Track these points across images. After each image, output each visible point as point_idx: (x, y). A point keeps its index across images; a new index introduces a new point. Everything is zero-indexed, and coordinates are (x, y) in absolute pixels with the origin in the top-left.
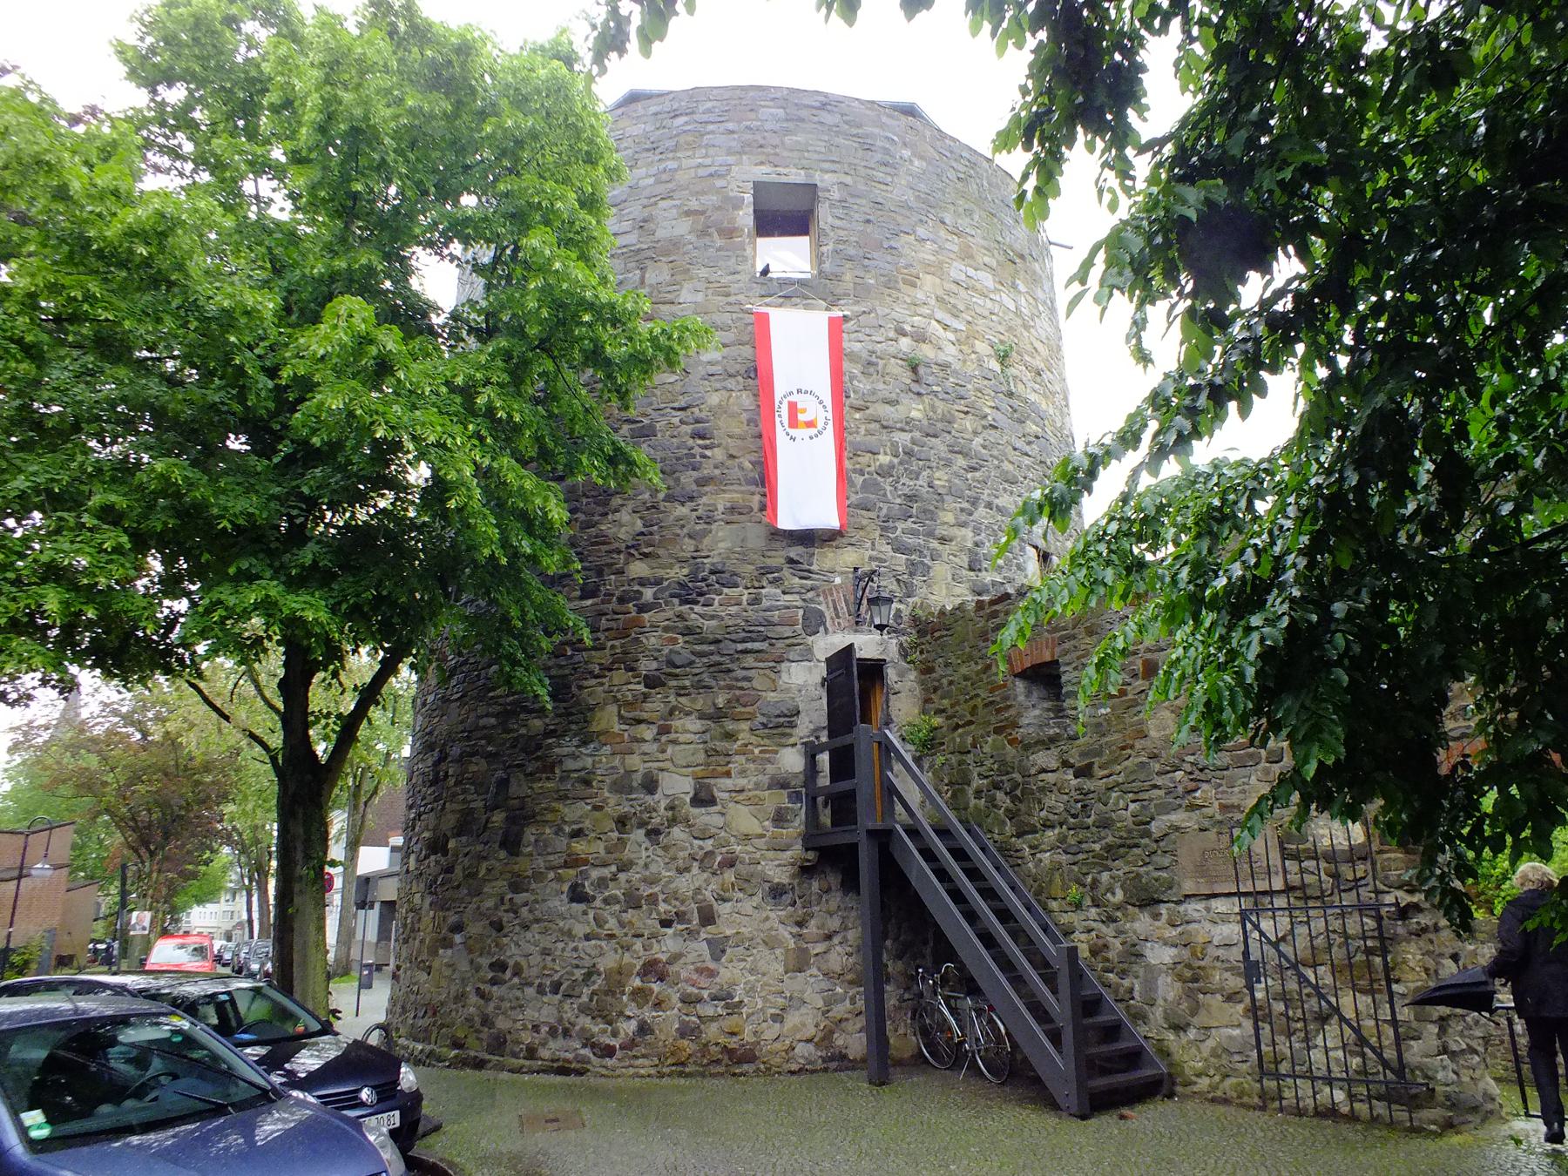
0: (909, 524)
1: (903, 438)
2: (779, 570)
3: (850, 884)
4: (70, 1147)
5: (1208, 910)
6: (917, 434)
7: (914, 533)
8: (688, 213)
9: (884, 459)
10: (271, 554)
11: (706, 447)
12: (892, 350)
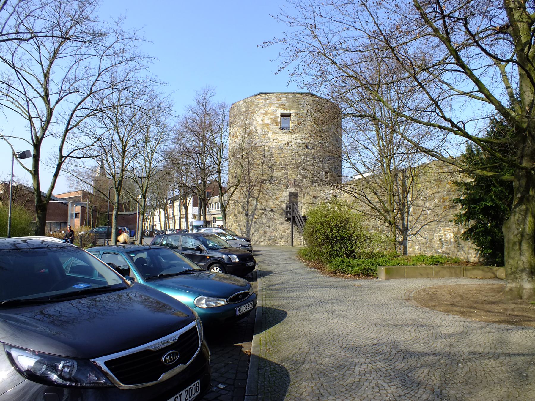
0: (303, 171)
9: (300, 161)
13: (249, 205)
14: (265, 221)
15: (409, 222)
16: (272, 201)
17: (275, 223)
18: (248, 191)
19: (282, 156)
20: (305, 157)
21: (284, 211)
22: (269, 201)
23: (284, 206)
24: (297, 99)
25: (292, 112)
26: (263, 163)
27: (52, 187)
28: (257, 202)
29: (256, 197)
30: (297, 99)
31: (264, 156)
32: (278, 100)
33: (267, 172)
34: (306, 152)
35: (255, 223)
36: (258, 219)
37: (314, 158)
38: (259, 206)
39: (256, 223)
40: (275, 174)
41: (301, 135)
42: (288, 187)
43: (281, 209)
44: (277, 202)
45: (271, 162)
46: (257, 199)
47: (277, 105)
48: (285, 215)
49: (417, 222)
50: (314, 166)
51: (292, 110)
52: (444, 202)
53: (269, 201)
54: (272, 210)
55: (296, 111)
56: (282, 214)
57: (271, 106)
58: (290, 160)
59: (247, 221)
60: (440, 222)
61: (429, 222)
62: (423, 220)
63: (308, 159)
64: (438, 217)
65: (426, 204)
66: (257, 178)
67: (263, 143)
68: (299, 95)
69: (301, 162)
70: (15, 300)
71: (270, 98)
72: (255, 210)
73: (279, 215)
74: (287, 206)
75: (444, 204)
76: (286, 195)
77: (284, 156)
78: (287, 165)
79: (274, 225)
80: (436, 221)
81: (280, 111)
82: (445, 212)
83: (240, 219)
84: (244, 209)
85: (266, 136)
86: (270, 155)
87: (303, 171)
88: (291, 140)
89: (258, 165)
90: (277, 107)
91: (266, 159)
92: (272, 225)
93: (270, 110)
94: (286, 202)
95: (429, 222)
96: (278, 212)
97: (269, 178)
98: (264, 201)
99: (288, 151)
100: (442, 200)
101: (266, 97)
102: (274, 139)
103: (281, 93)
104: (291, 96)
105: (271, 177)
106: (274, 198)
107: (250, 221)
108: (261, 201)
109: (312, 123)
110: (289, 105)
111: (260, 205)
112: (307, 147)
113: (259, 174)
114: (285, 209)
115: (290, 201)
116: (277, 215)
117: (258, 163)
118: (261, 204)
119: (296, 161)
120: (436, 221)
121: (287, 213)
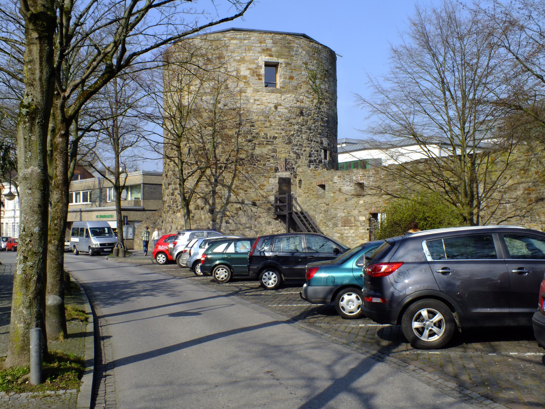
0: (297, 148)
1: (296, 127)
2: (269, 158)
3: (285, 222)
4: (113, 282)
5: (20, 27)
6: (300, 126)
7: (298, 149)
8: (249, 69)
9: (292, 133)
10: (32, 113)
11: (254, 129)
12: (295, 106)
13: (216, 196)
14: (244, 220)
15: (480, 218)
16: (254, 190)
17: (259, 223)
18: (214, 176)
19: (268, 124)
20: (299, 128)
21: (272, 205)
22: (248, 190)
23: (272, 199)
24: (288, 43)
25: (280, 61)
26: (238, 134)
27: (125, 183)
28: (229, 192)
29: (227, 184)
30: (288, 43)
31: (240, 124)
32: (261, 43)
33: (246, 148)
34: (300, 119)
35: (227, 222)
36: (233, 217)
37: (310, 129)
38: (233, 198)
39: (229, 223)
40: (258, 151)
41: (293, 96)
42: (276, 170)
43: (269, 202)
44: (261, 191)
45: (252, 134)
46: (230, 188)
47: (259, 49)
48: (273, 210)
49: (492, 218)
50: (311, 141)
51: (282, 58)
52: (530, 194)
53: (248, 190)
54: (254, 204)
55: (287, 60)
56: (269, 209)
57: (249, 50)
58: (279, 132)
59: (214, 220)
60: (524, 217)
61: (509, 218)
62: (501, 215)
63: (303, 131)
64: (521, 211)
65: (504, 196)
66: (230, 156)
67: (238, 105)
68: (290, 38)
69: (294, 134)
70: (493, 313)
71: (249, 38)
72: (227, 203)
73: (264, 211)
74: (276, 199)
75: (530, 196)
76: (273, 182)
77: (271, 125)
78: (275, 138)
79: (258, 226)
80: (518, 216)
81: (263, 59)
82: (531, 206)
83: (201, 218)
84: (206, 201)
85: (243, 94)
86: (249, 123)
87: (297, 148)
88: (280, 102)
89: (231, 137)
90: (259, 52)
91: (244, 129)
92: (255, 226)
93: (249, 55)
94: (274, 192)
95: (509, 218)
96: (263, 207)
97: (248, 156)
98: (241, 191)
99: (275, 119)
100: (526, 192)
101: (242, 36)
102: (255, 100)
103: (266, 32)
104: (278, 37)
105: (252, 155)
106: (257, 186)
107: (218, 221)
108: (236, 190)
109: (308, 79)
110: (277, 51)
111: (235, 197)
112: (302, 113)
113: (233, 151)
114: (273, 203)
115: (281, 191)
116: (262, 210)
117: (230, 133)
118: (237, 195)
119: (288, 133)
120: (518, 216)
121: (276, 207)
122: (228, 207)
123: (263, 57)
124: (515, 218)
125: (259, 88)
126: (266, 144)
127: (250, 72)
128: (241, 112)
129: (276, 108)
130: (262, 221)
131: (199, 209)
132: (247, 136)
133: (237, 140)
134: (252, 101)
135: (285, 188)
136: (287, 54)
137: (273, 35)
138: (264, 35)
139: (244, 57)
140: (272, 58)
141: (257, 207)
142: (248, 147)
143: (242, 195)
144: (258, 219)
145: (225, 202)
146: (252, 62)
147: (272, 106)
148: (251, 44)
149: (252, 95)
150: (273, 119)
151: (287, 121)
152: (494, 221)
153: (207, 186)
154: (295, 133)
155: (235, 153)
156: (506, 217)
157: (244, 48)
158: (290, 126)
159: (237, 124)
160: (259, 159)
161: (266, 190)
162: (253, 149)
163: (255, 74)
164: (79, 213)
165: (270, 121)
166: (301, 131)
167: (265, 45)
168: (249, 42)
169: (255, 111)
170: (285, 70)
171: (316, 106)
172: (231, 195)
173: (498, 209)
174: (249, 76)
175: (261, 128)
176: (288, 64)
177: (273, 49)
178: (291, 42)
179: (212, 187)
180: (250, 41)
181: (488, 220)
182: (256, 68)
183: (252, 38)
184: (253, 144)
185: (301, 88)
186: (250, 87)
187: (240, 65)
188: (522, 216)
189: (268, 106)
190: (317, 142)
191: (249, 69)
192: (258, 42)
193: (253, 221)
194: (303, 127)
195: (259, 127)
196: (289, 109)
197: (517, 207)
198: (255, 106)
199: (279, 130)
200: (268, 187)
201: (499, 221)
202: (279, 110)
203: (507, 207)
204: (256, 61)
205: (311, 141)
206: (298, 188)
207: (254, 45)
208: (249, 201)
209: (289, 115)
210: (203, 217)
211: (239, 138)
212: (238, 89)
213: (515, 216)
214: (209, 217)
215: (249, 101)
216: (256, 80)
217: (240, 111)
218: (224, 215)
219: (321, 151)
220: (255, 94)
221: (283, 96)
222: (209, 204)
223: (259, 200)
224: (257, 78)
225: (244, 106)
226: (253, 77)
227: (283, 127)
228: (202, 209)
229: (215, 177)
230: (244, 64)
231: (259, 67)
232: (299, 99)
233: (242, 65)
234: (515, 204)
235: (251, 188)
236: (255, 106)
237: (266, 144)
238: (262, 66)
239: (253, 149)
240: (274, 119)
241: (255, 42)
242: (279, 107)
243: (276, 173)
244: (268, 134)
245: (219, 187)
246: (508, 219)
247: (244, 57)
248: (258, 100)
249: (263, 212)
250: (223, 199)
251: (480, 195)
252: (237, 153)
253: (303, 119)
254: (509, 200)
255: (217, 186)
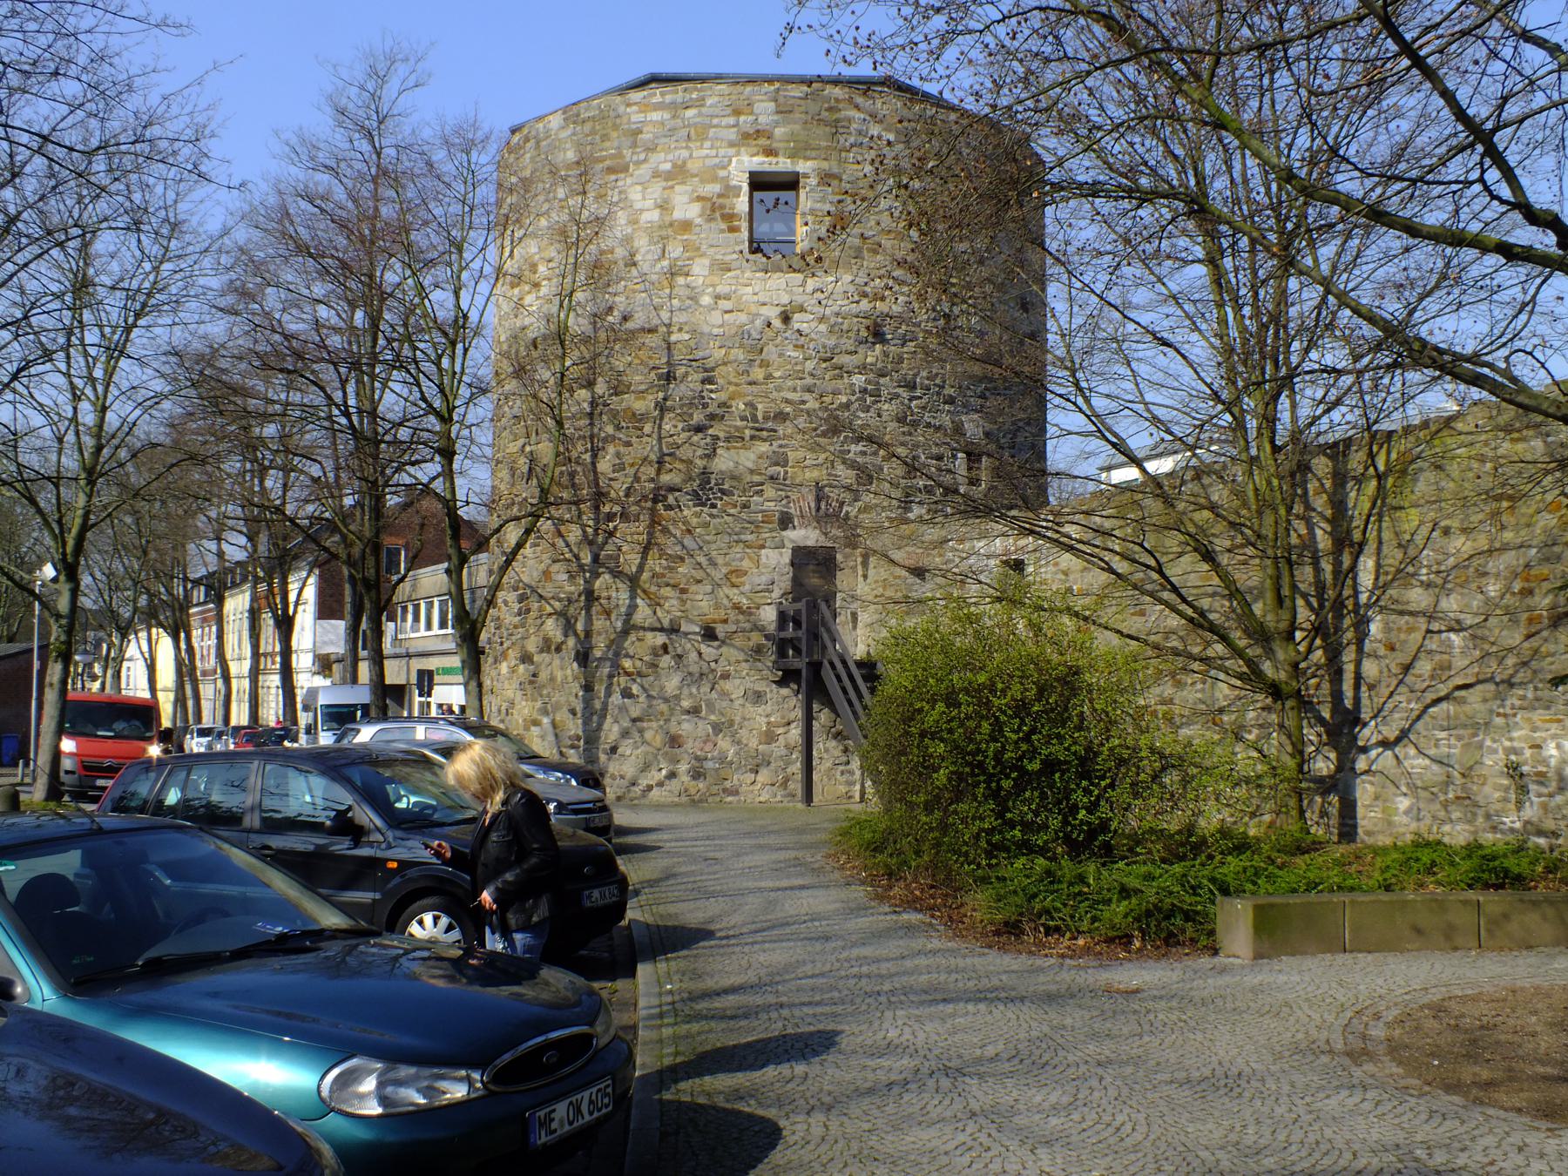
0: (860, 448)
2: (762, 484)
7: (864, 453)
8: (699, 199)
13: (596, 609)
15: (1364, 688)
17: (724, 694)
19: (758, 373)
20: (868, 382)
21: (767, 637)
23: (769, 615)
24: (830, 109)
25: (802, 166)
26: (662, 408)
28: (633, 597)
29: (627, 570)
30: (830, 109)
32: (737, 113)
34: (873, 355)
35: (627, 694)
38: (643, 613)
40: (724, 461)
41: (848, 278)
42: (785, 522)
43: (757, 628)
45: (705, 406)
46: (634, 581)
47: (732, 134)
48: (770, 658)
49: (1402, 689)
51: (807, 158)
52: (1531, 592)
54: (709, 634)
55: (825, 165)
56: (758, 650)
57: (702, 138)
59: (588, 688)
60: (1512, 685)
62: (1432, 677)
67: (665, 315)
68: (837, 91)
72: (625, 632)
75: (1530, 601)
76: (774, 562)
77: (769, 377)
80: (1491, 679)
81: (749, 161)
82: (1535, 642)
84: (569, 627)
85: (681, 280)
88: (799, 299)
90: (732, 144)
91: (679, 391)
92: (710, 705)
93: (701, 155)
94: (776, 594)
98: (666, 591)
99: (784, 355)
100: (1517, 587)
102: (718, 297)
103: (752, 80)
105: (705, 474)
107: (600, 689)
108: (653, 589)
110: (792, 137)
111: (648, 611)
112: (877, 335)
114: (772, 628)
115: (798, 588)
117: (640, 406)
119: (828, 399)
120: (1491, 679)
121: (782, 646)
122: (630, 644)
123: (746, 158)
124: (1479, 687)
125: (728, 258)
126: (752, 438)
127: (703, 208)
128: (674, 338)
129: (786, 319)
130: (735, 688)
131: (549, 651)
132: (691, 415)
133: (660, 427)
134: (706, 300)
135: (814, 581)
136: (824, 144)
137: (777, 85)
138: (749, 89)
139: (684, 162)
140: (774, 160)
141: (716, 643)
142: (693, 449)
143: (671, 606)
144: (722, 682)
145: (619, 624)
146: (710, 175)
147: (772, 313)
148: (707, 120)
149: (708, 282)
150: (774, 357)
151: (825, 361)
152: (1409, 702)
153: (572, 577)
154: (853, 398)
155: (652, 472)
156: (1451, 684)
157: (684, 132)
158: (834, 378)
159: (660, 377)
160: (726, 487)
161: (747, 587)
162: (708, 456)
163: (717, 215)
164: (404, 661)
165: (765, 364)
166: (876, 394)
167: (751, 118)
168: (700, 114)
169: (716, 331)
170: (818, 195)
171: (934, 310)
172: (636, 606)
173: (1422, 655)
174: (698, 221)
175: (737, 385)
176: (826, 178)
177: (779, 132)
178: (841, 106)
179: (586, 581)
180: (704, 110)
181: (1392, 694)
182: (720, 196)
183: (709, 102)
184: (708, 440)
185: (875, 252)
186: (703, 255)
187: (672, 187)
188: (1503, 681)
189: (758, 315)
190: (938, 428)
191: (699, 199)
192: (729, 111)
193: (706, 688)
194: (882, 381)
195: (730, 383)
196: (833, 320)
197: (1486, 647)
198: (716, 318)
199: (795, 390)
200: (758, 579)
201: (1428, 701)
202: (796, 326)
203: (1451, 646)
204: (722, 173)
205: (915, 424)
206: (861, 579)
207: (715, 121)
208: (692, 622)
209: (832, 342)
210: (559, 675)
211: (666, 420)
212: (665, 263)
213: (1479, 682)
214: (576, 678)
215: (697, 302)
216: (722, 231)
217: (670, 333)
218: (616, 665)
219: (954, 457)
220: (716, 279)
221: (810, 281)
222: (576, 634)
223: (725, 621)
224: (724, 226)
225: (680, 318)
226: (713, 225)
227: (809, 381)
228: (558, 649)
229: (595, 548)
230: (683, 183)
231: (730, 191)
232: (868, 289)
233: (678, 188)
234: (1479, 632)
235: (699, 582)
236: (716, 318)
237: (752, 438)
238: (740, 188)
239: (708, 456)
240: (781, 355)
241: (717, 111)
242: (797, 316)
243: (784, 533)
244: (760, 407)
245: (605, 578)
246: (1457, 694)
247: (684, 162)
248: (727, 297)
249: (738, 662)
250: (613, 617)
251: (1363, 598)
252: (659, 472)
253: (886, 354)
254: (1462, 616)
255: (598, 575)
